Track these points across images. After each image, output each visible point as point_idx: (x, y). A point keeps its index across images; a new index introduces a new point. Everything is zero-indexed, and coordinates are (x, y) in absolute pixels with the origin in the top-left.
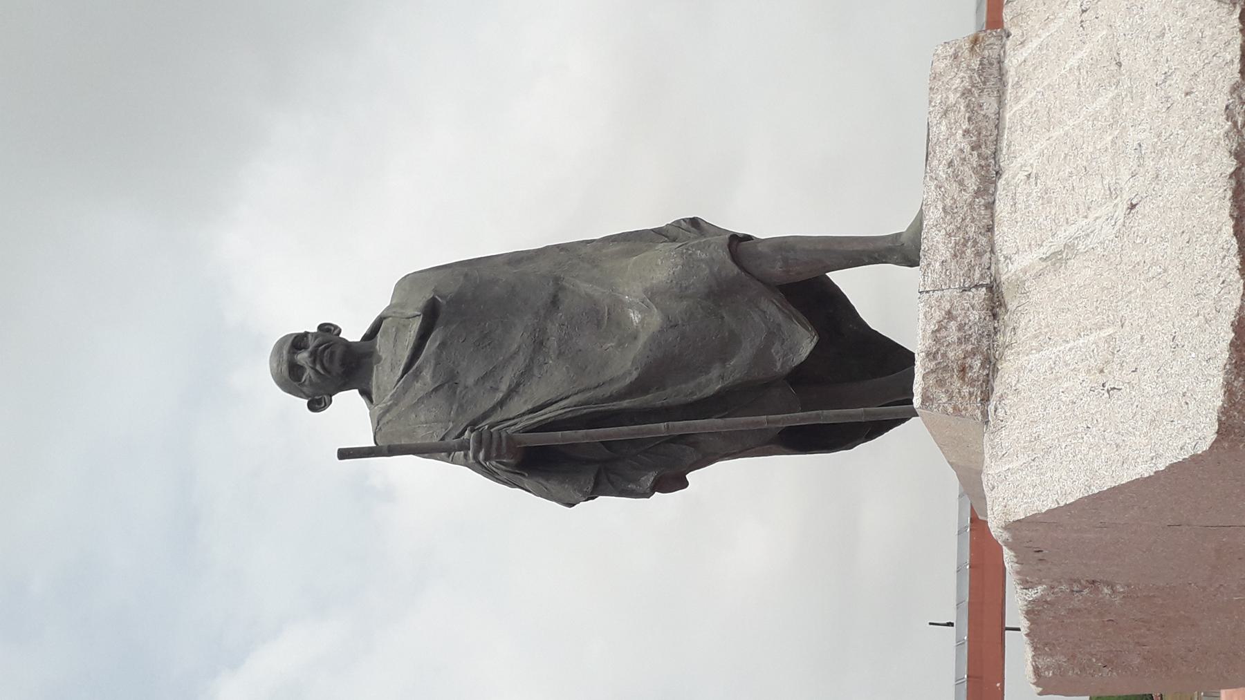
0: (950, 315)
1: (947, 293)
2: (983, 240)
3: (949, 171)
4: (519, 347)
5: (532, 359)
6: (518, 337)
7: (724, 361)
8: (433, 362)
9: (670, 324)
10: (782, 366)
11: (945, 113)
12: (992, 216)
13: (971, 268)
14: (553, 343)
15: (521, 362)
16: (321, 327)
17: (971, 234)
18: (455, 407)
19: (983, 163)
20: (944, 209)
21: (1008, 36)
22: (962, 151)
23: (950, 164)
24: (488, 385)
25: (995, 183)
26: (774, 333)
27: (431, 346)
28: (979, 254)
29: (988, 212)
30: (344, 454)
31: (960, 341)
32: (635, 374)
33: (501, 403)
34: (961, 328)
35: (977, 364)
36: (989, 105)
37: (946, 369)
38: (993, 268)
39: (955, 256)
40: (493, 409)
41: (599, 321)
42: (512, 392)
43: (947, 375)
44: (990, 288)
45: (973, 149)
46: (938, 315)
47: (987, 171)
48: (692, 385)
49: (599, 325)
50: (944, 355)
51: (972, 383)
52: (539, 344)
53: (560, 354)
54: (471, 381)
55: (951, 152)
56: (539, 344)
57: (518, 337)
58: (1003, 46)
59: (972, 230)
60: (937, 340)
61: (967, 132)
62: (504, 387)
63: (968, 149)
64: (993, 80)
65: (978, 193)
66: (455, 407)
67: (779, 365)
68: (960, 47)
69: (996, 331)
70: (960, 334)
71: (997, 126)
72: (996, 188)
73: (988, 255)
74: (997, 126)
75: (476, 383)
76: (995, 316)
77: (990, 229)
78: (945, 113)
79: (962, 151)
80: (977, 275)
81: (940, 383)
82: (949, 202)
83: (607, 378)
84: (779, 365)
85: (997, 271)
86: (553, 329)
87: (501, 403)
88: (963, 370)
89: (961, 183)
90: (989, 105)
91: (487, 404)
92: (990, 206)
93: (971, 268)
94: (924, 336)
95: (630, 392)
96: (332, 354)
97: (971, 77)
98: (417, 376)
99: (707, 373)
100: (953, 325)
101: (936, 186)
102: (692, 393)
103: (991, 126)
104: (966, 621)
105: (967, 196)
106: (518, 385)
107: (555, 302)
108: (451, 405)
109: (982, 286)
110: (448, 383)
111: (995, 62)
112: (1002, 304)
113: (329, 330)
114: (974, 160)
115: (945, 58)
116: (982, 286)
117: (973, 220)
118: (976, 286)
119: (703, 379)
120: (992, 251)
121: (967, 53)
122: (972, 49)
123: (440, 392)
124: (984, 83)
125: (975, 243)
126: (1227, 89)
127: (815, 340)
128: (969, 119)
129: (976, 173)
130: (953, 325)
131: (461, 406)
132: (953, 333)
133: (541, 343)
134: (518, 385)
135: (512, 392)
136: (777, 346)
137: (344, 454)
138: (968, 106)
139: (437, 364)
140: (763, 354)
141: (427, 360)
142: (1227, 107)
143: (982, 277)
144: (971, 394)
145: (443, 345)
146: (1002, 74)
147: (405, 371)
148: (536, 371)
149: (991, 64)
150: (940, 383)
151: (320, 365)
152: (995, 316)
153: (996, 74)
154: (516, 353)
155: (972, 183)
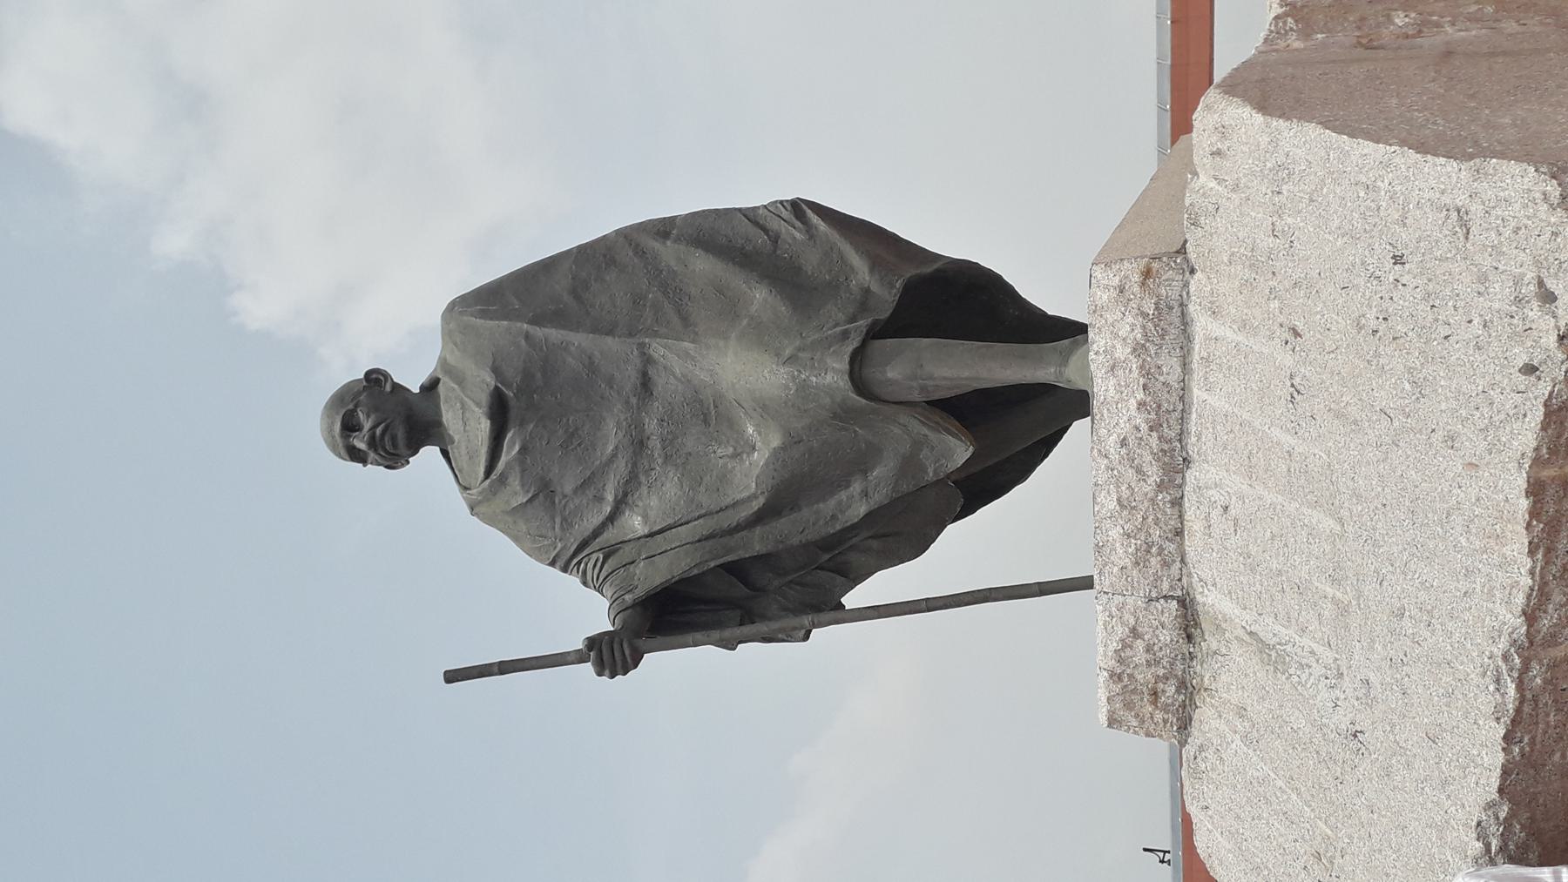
0: (1135, 633)
1: (1130, 600)
2: (1172, 547)
3: (1124, 451)
5: (635, 465)
6: (611, 436)
7: (865, 472)
8: (517, 469)
9: (793, 439)
10: (935, 471)
11: (1113, 368)
13: (1158, 578)
14: (655, 443)
15: (621, 467)
16: (368, 374)
17: (1156, 539)
18: (558, 520)
19: (1166, 447)
20: (1119, 500)
21: (1192, 271)
24: (591, 493)
25: (1182, 472)
26: (918, 444)
27: (510, 451)
28: (1166, 564)
30: (452, 677)
32: (762, 500)
33: (611, 519)
34: (1148, 649)
35: (1171, 690)
36: (1170, 367)
37: (1134, 691)
38: (1184, 580)
42: (620, 505)
43: (1135, 698)
44: (1182, 602)
45: (1151, 429)
46: (1121, 631)
47: (1172, 457)
48: (832, 503)
49: (706, 422)
50: (1131, 676)
51: (1165, 709)
52: (639, 445)
53: (667, 458)
54: (568, 488)
55: (1124, 428)
56: (639, 445)
57: (611, 436)
58: (1186, 285)
59: (1156, 533)
60: (1121, 661)
61: (1141, 405)
62: (610, 498)
63: (1144, 427)
65: (1161, 487)
66: (558, 520)
68: (1126, 277)
71: (1182, 398)
72: (1183, 478)
73: (1178, 565)
74: (1182, 398)
75: (575, 491)
76: (1189, 638)
77: (1179, 533)
78: (1113, 368)
79: (1137, 428)
80: (1165, 586)
81: (1129, 706)
82: (1125, 493)
83: (729, 501)
86: (651, 425)
87: (611, 519)
88: (1155, 694)
89: (1139, 471)
90: (1170, 367)
91: (595, 520)
92: (1178, 503)
93: (1158, 578)
94: (1105, 655)
95: (759, 518)
97: (1144, 327)
98: (503, 479)
99: (848, 486)
100: (1140, 645)
101: (1107, 468)
103: (1174, 398)
105: (1148, 488)
106: (625, 495)
107: (646, 385)
108: (553, 519)
109: (1172, 597)
110: (544, 492)
111: (1176, 305)
112: (1197, 625)
113: (377, 381)
114: (1154, 441)
115: (1107, 287)
116: (1172, 597)
117: (1157, 521)
119: (843, 495)
120: (1183, 561)
121: (1136, 289)
122: (1143, 284)
123: (536, 503)
124: (1162, 337)
128: (1145, 387)
129: (1158, 460)
130: (1140, 645)
131: (564, 519)
132: (1139, 654)
133: (641, 443)
134: (625, 495)
135: (620, 505)
136: (925, 451)
137: (452, 677)
138: (1142, 367)
139: (523, 471)
140: (909, 464)
142: (1479, 824)
143: (1172, 588)
144: (1165, 721)
146: (1185, 322)
148: (643, 479)
149: (1171, 308)
151: (384, 422)
152: (1189, 638)
153: (1177, 321)
154: (614, 455)
155: (1154, 474)
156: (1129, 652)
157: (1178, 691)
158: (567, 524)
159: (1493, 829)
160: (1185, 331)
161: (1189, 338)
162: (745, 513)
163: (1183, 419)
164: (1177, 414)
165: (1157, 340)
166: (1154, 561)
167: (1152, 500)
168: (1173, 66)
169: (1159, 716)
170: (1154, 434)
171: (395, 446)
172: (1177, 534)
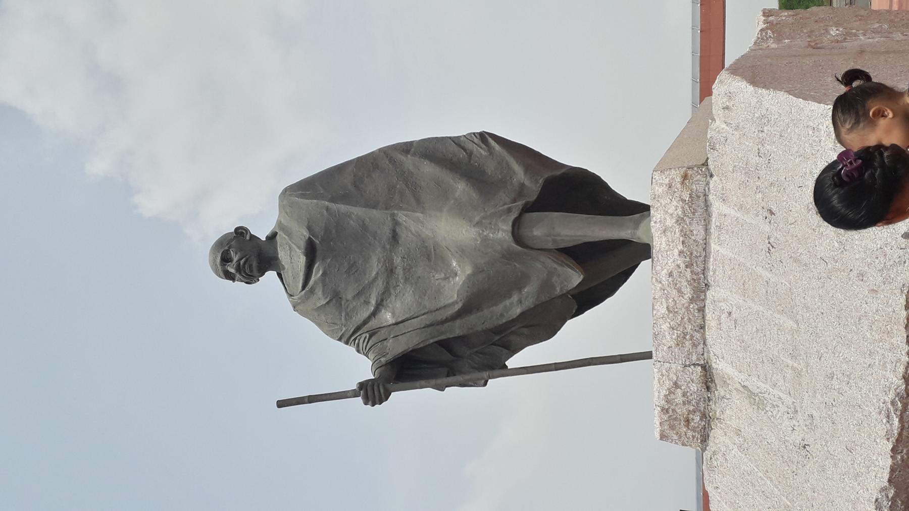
1: (673, 366)
2: (698, 335)
3: (670, 279)
4: (377, 273)
5: (387, 283)
6: (375, 266)
10: (561, 289)
12: (704, 318)
13: (690, 353)
14: (399, 271)
15: (380, 285)
16: (237, 229)
18: (343, 314)
19: (695, 277)
20: (667, 308)
21: (711, 176)
22: (678, 266)
23: (670, 274)
24: (362, 299)
25: (704, 292)
27: (317, 274)
28: (695, 345)
29: (700, 314)
30: (281, 404)
31: (684, 403)
33: (374, 314)
34: (684, 395)
35: (697, 419)
36: (698, 231)
37: (675, 419)
39: (678, 345)
40: (369, 319)
41: (429, 255)
43: (676, 423)
45: (687, 267)
46: (668, 384)
47: (699, 283)
49: (429, 259)
51: (694, 430)
52: (390, 271)
53: (406, 280)
54: (350, 297)
55: (671, 266)
56: (390, 271)
57: (375, 266)
58: (708, 184)
59: (689, 327)
60: (668, 401)
61: (681, 252)
62: (373, 302)
63: (683, 266)
64: (700, 211)
65: (692, 300)
66: (343, 314)
67: (558, 289)
68: (673, 179)
69: (709, 399)
70: (684, 399)
71: (704, 249)
72: (705, 295)
73: (702, 346)
74: (704, 249)
75: (354, 298)
76: (708, 388)
77: (702, 327)
78: (664, 232)
79: (678, 266)
80: (694, 358)
81: (672, 427)
82: (671, 304)
83: (442, 304)
84: (558, 289)
85: (709, 357)
86: (397, 260)
87: (374, 314)
88: (688, 421)
89: (679, 291)
90: (698, 231)
91: (364, 314)
92: (702, 310)
93: (690, 353)
94: (659, 397)
95: (459, 315)
96: (251, 266)
98: (312, 291)
100: (679, 392)
101: (661, 289)
102: (502, 315)
103: (700, 249)
104: (698, 69)
106: (382, 300)
108: (340, 313)
109: (698, 365)
110: (336, 298)
111: (702, 195)
112: (713, 381)
114: (688, 274)
116: (698, 365)
118: (694, 364)
119: (507, 302)
120: (704, 343)
121: (679, 186)
122: (683, 183)
123: (331, 304)
124: (694, 213)
125: (692, 336)
126: (878, 488)
127: (582, 277)
128: (683, 242)
129: (691, 285)
130: (679, 392)
131: (347, 314)
132: (679, 399)
133: (392, 270)
134: (382, 300)
137: (281, 404)
138: (682, 231)
139: (324, 286)
141: (315, 282)
142: (877, 500)
143: (698, 359)
144: (693, 437)
145: (325, 274)
146: (707, 205)
147: (304, 287)
148: (392, 291)
149: (699, 197)
150: (672, 427)
151: (244, 256)
152: (708, 388)
153: (702, 205)
154: (376, 278)
155: (688, 292)
156: (672, 396)
157: (701, 419)
158: (348, 317)
159: (885, 503)
160: (707, 210)
161: (710, 215)
162: (450, 312)
163: (705, 261)
164: (702, 259)
165: (691, 215)
166: (688, 344)
167: (687, 308)
168: (701, 57)
169: (690, 434)
170: (688, 270)
171: (251, 271)
172: (701, 328)
